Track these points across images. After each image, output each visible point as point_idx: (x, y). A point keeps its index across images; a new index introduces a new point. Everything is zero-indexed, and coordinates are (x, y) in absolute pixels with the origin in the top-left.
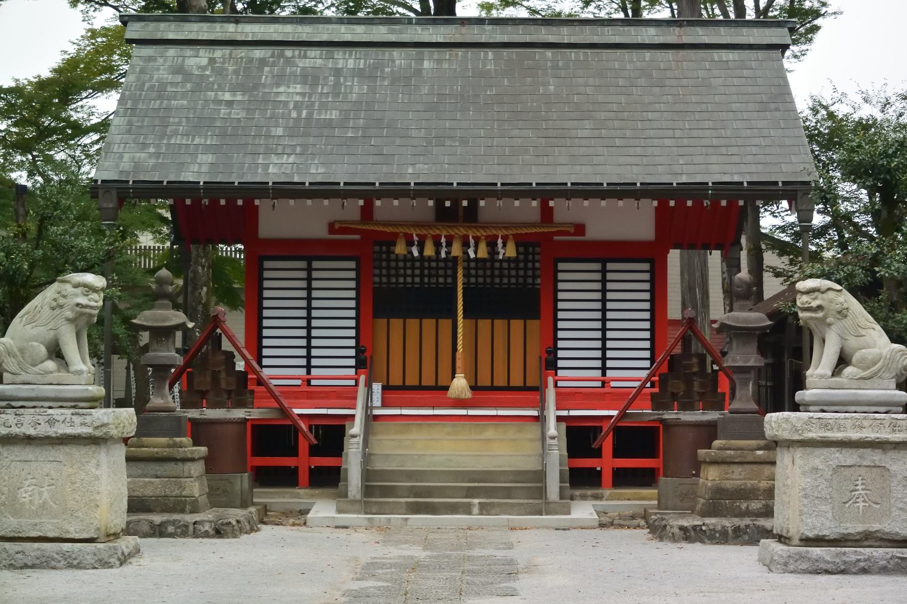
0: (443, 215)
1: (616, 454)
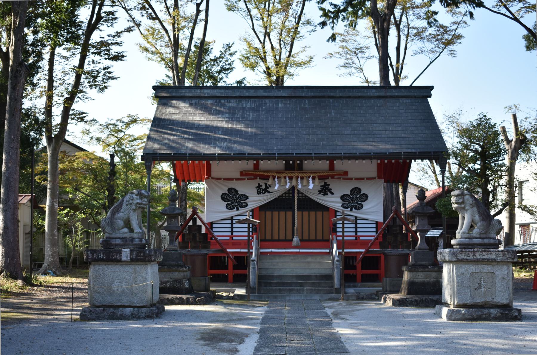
0: (289, 168)
1: (363, 268)
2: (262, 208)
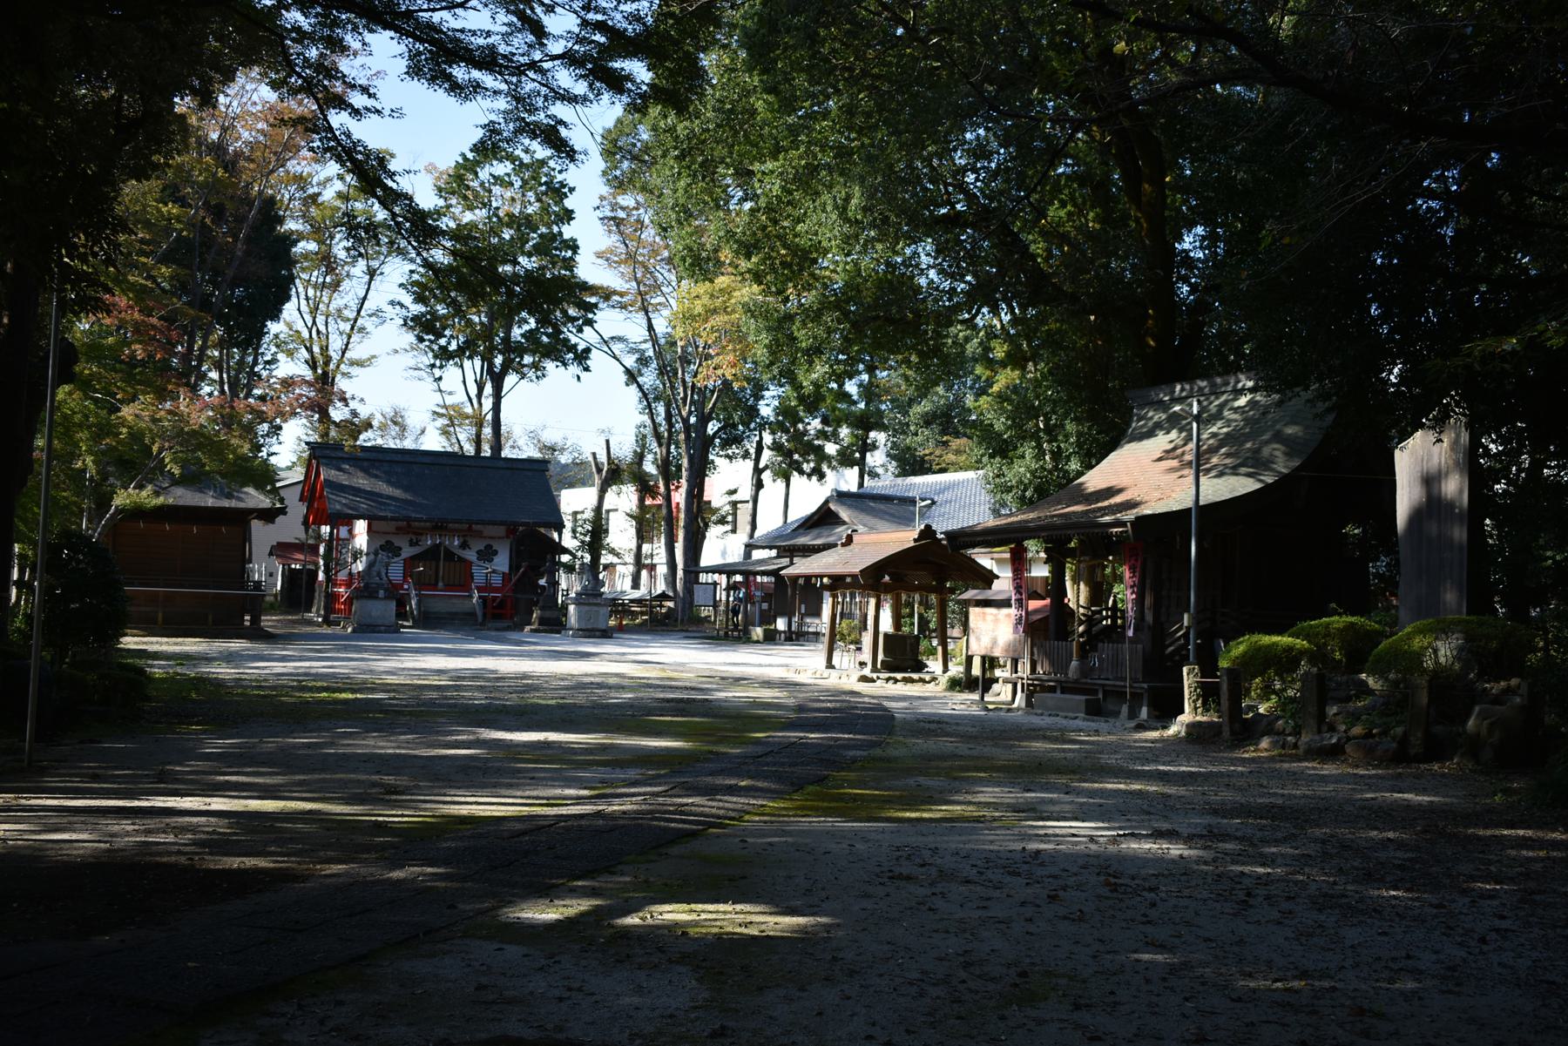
2: (412, 558)
